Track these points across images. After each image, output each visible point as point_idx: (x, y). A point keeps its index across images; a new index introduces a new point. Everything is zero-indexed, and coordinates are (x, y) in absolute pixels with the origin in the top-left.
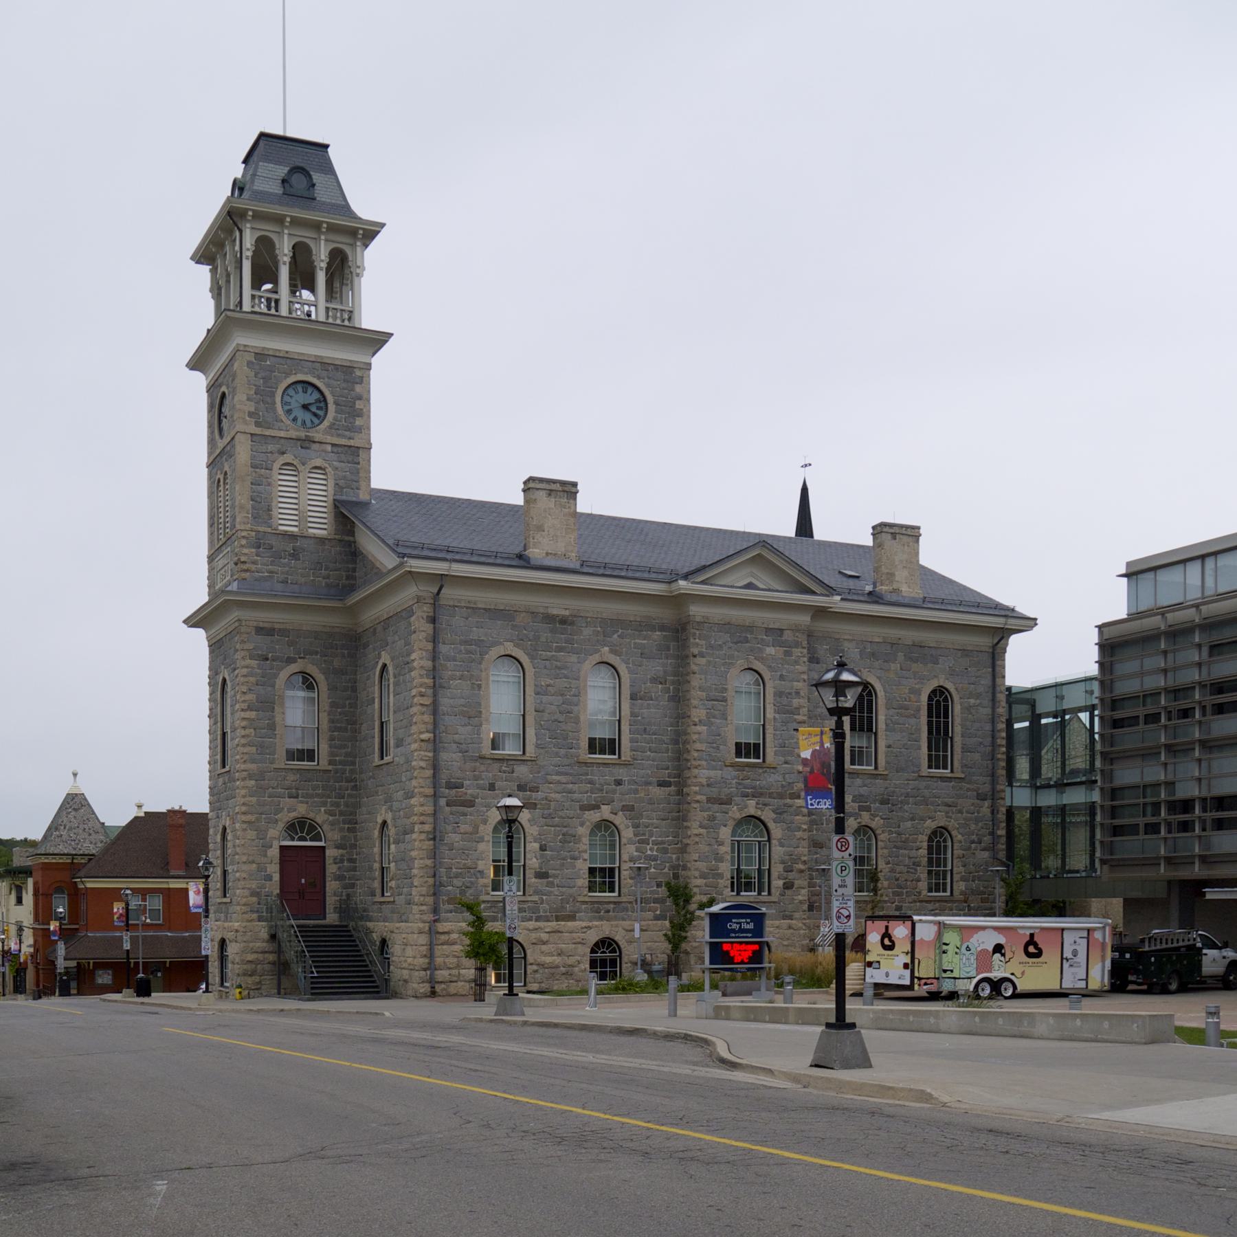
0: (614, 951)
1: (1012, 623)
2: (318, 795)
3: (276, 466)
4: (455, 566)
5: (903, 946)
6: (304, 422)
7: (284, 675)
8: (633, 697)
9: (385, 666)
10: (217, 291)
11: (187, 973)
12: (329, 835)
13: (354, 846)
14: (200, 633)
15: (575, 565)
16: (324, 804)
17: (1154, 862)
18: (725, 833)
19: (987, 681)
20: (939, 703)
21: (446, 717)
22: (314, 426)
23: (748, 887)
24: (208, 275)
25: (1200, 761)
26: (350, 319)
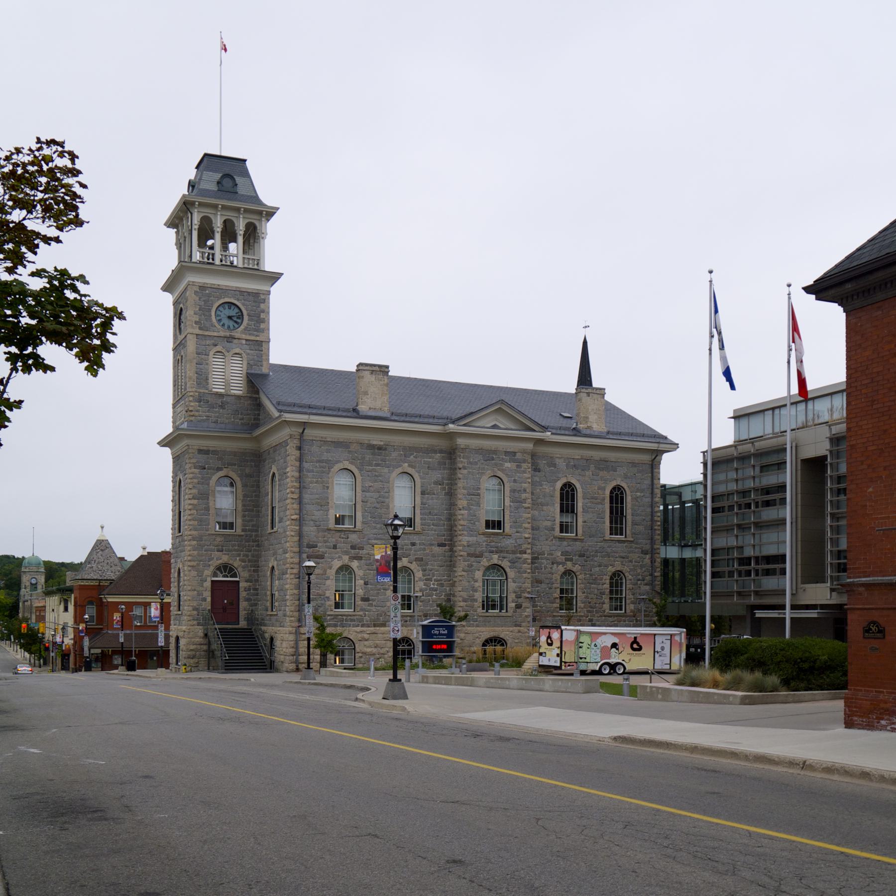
0: (410, 645)
1: (662, 447)
2: (235, 550)
3: (211, 353)
4: (312, 417)
5: (557, 644)
6: (229, 327)
7: (215, 478)
8: (423, 493)
9: (274, 474)
10: (179, 245)
11: (158, 658)
12: (242, 574)
13: (257, 581)
14: (167, 451)
15: (387, 414)
16: (239, 555)
17: (730, 595)
18: (479, 575)
19: (648, 482)
20: (617, 496)
21: (307, 506)
22: (235, 328)
23: (494, 607)
24: (175, 235)
25: (754, 534)
26: (258, 264)
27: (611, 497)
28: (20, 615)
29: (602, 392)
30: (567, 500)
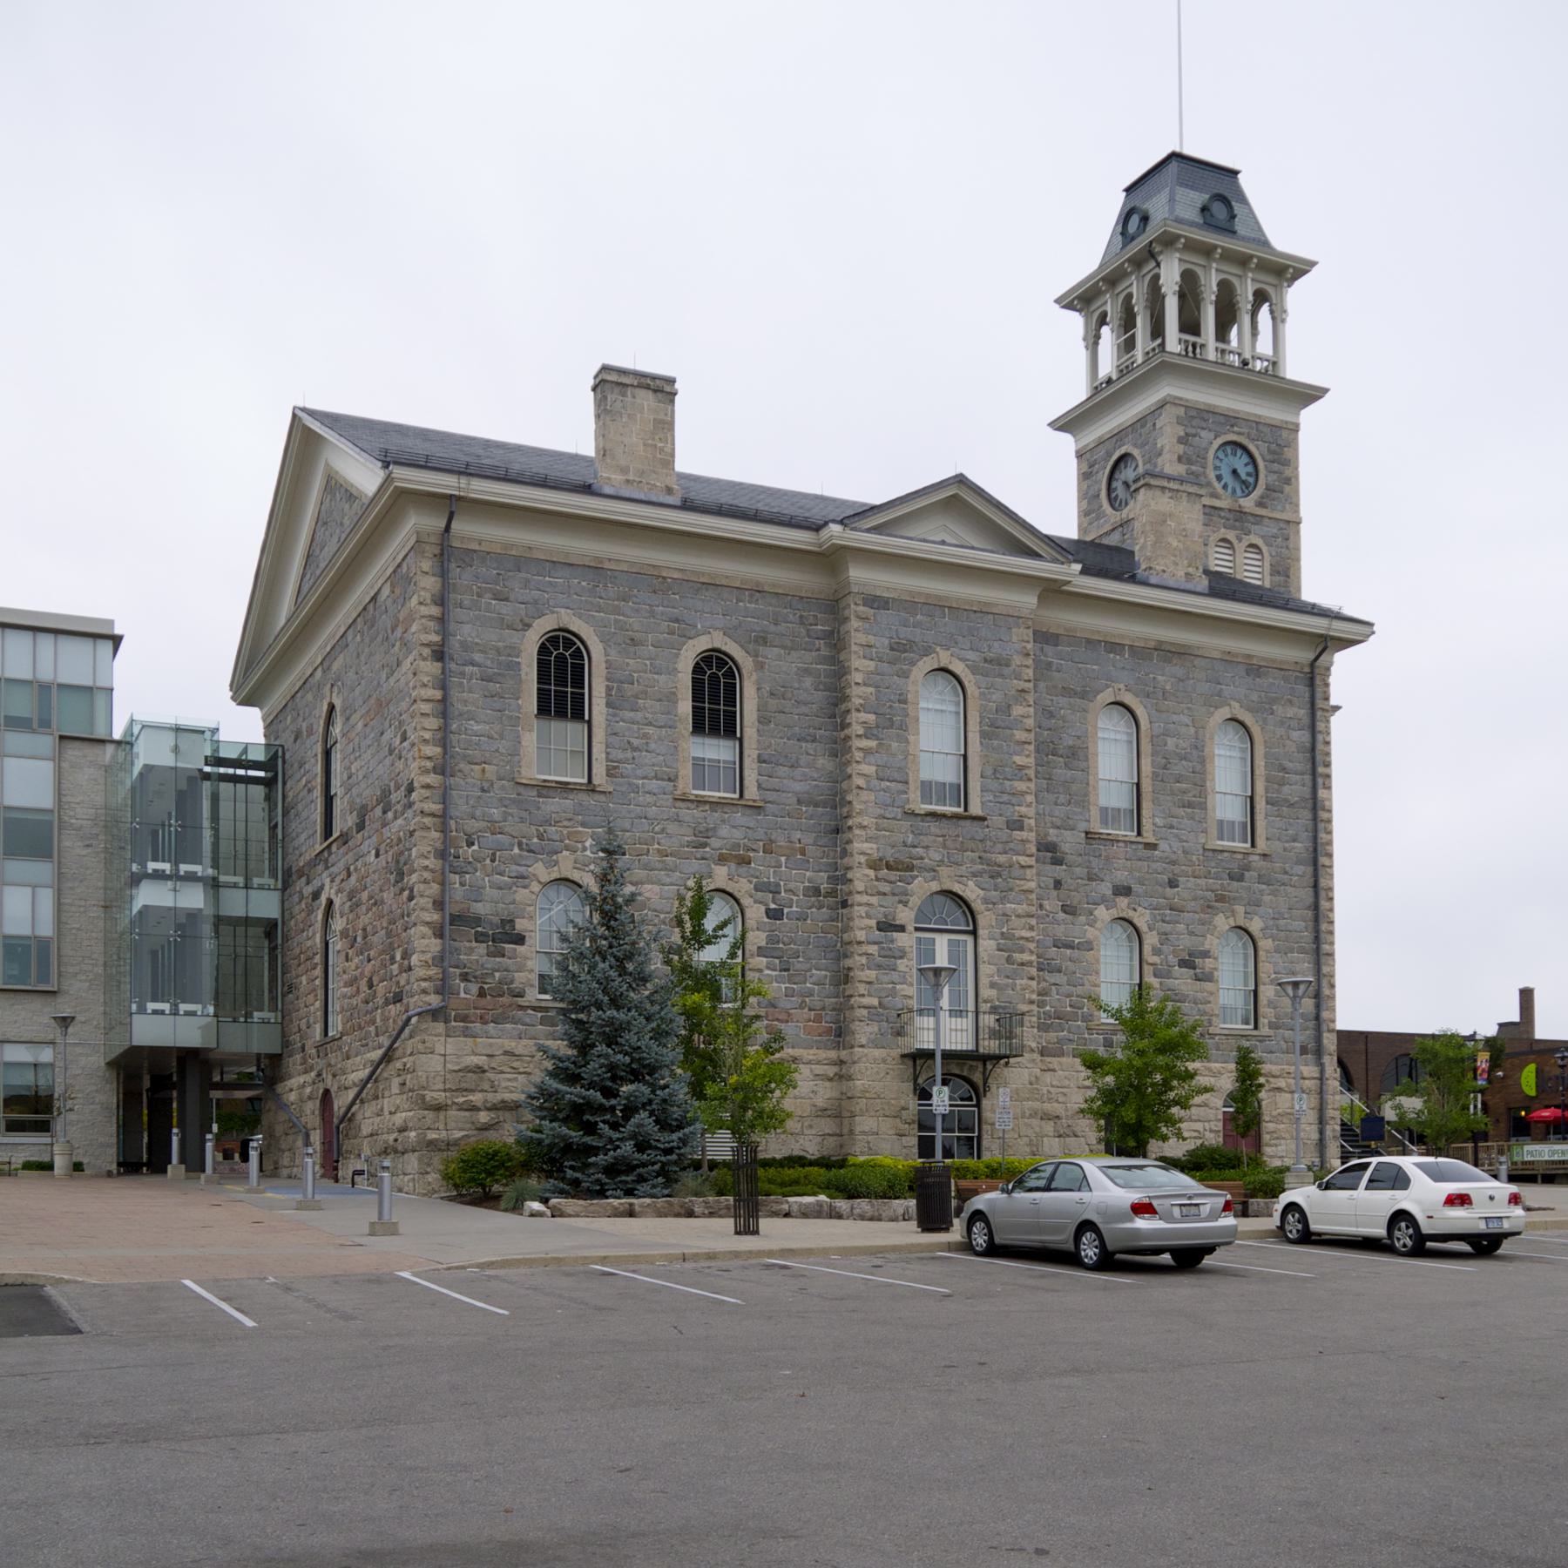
30: (714, 699)
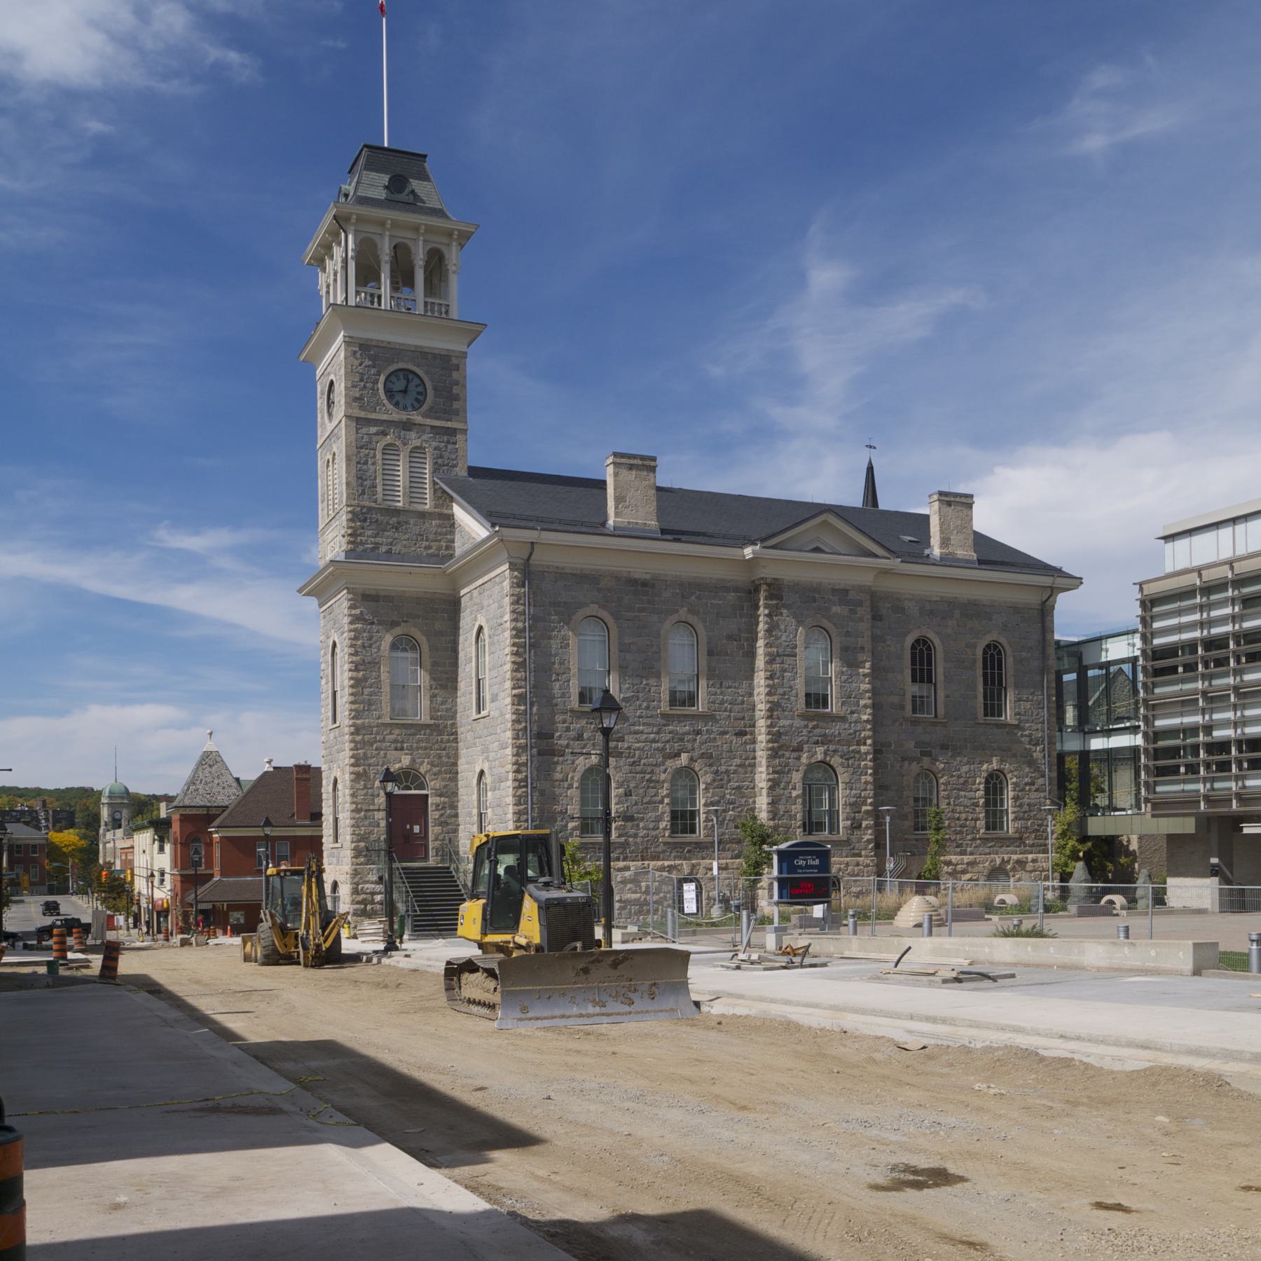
8: (710, 653)
9: (481, 628)
27: (985, 660)
28: (101, 861)
29: (968, 501)
30: (922, 664)
